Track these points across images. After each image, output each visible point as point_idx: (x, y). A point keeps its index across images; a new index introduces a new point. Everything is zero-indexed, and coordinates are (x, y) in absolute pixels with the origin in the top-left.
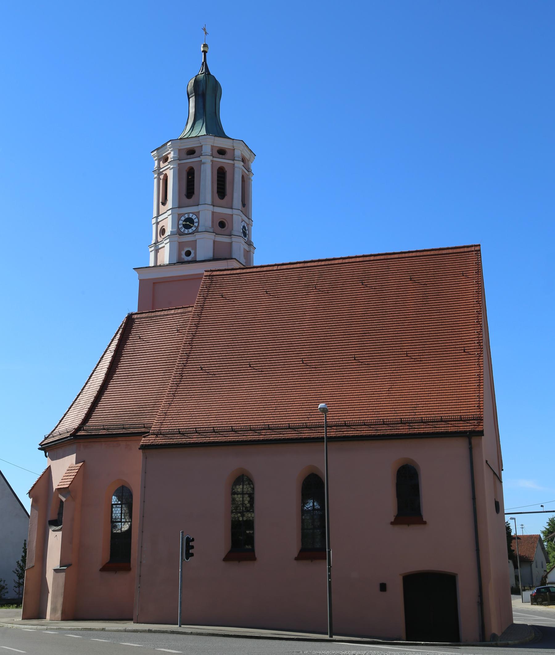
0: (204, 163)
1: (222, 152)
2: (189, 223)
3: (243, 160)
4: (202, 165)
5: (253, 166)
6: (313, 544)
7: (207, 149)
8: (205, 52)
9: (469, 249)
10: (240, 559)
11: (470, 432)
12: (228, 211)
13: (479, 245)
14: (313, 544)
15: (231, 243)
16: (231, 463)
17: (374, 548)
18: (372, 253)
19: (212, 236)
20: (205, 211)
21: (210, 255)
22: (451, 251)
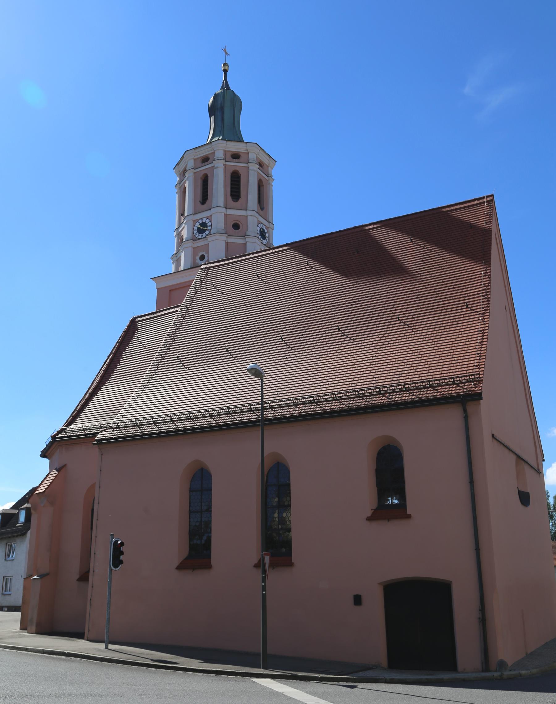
0: (217, 167)
1: (236, 156)
2: (202, 228)
3: (261, 165)
4: (215, 170)
5: (275, 172)
6: (277, 546)
7: (220, 154)
8: (225, 71)
9: (480, 201)
10: (194, 568)
11: (465, 396)
12: (243, 213)
13: (492, 195)
14: (277, 546)
15: (245, 244)
16: (186, 455)
17: (346, 552)
18: (372, 222)
19: (224, 237)
20: (218, 214)
21: (223, 256)
22: (459, 206)
